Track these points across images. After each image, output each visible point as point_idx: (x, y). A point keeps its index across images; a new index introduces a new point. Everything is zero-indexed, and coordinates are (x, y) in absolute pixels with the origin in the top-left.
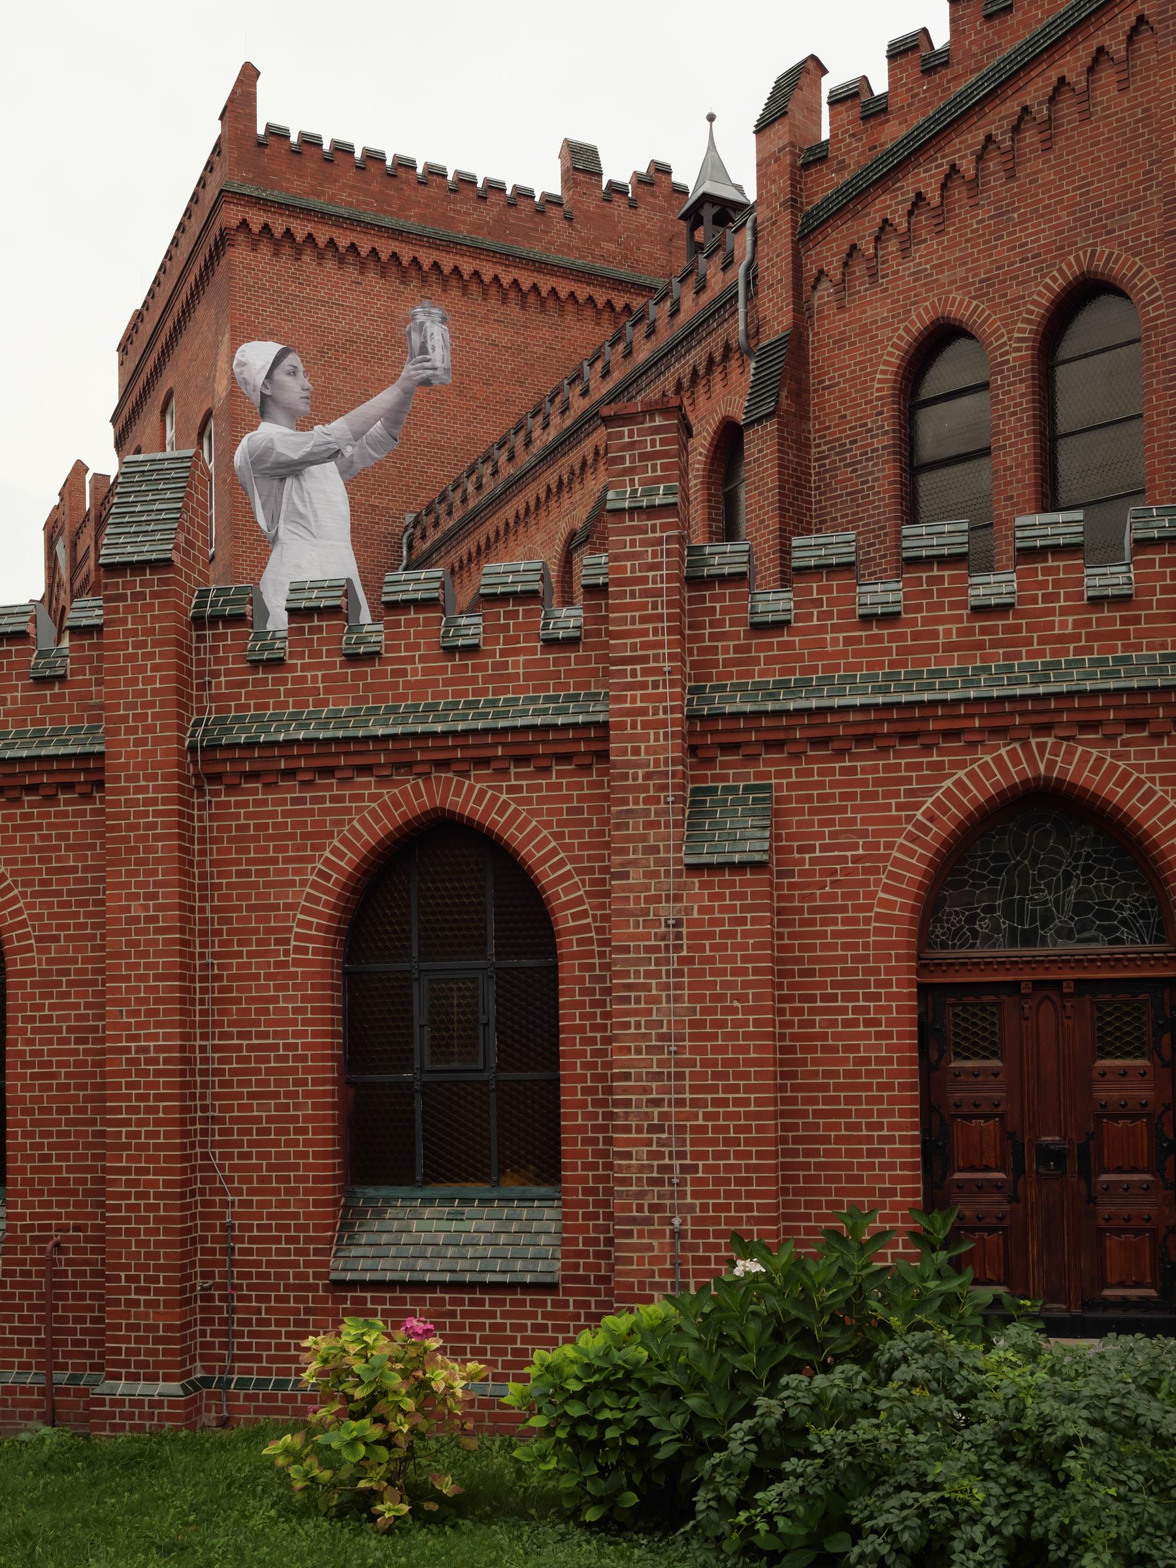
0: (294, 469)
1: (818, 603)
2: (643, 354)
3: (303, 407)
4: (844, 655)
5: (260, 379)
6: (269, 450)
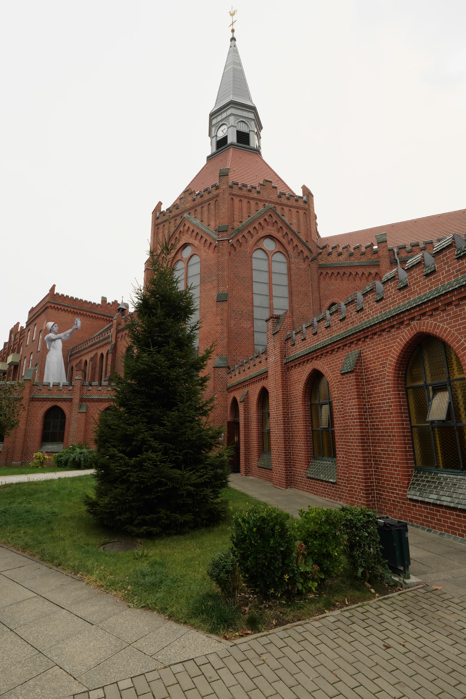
2: (101, 338)
6: (50, 337)
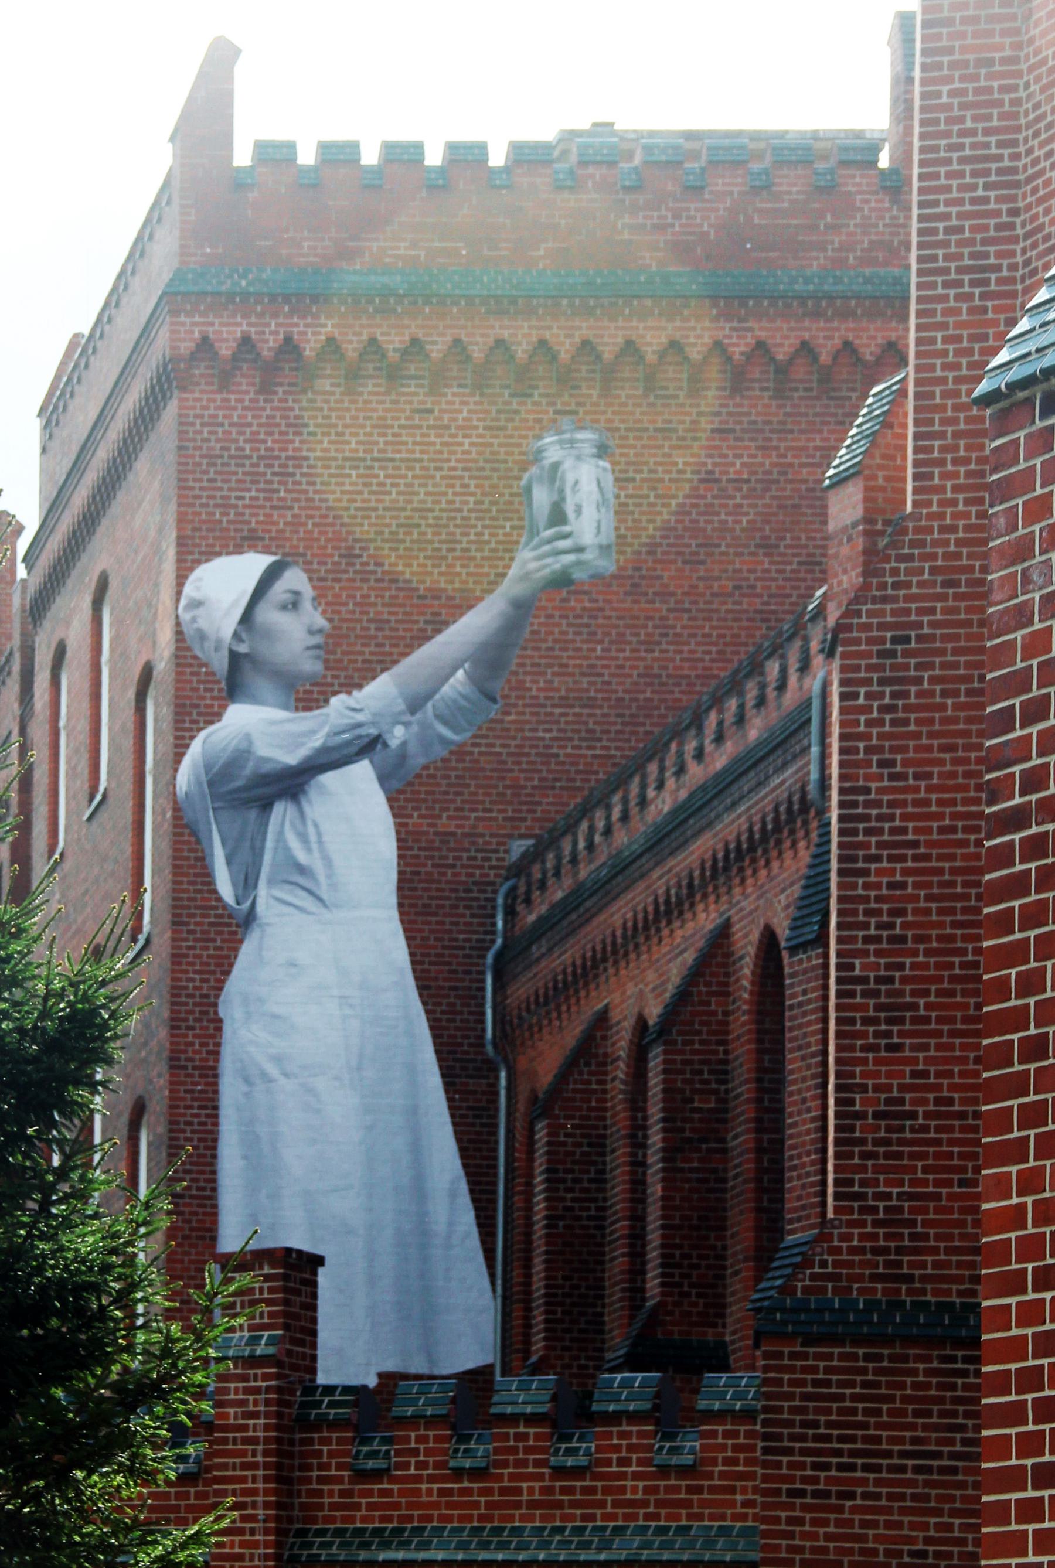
0: (291, 783)
1: (415, 1452)
3: (311, 666)
4: (436, 1505)
5: (228, 626)
6: (240, 756)
